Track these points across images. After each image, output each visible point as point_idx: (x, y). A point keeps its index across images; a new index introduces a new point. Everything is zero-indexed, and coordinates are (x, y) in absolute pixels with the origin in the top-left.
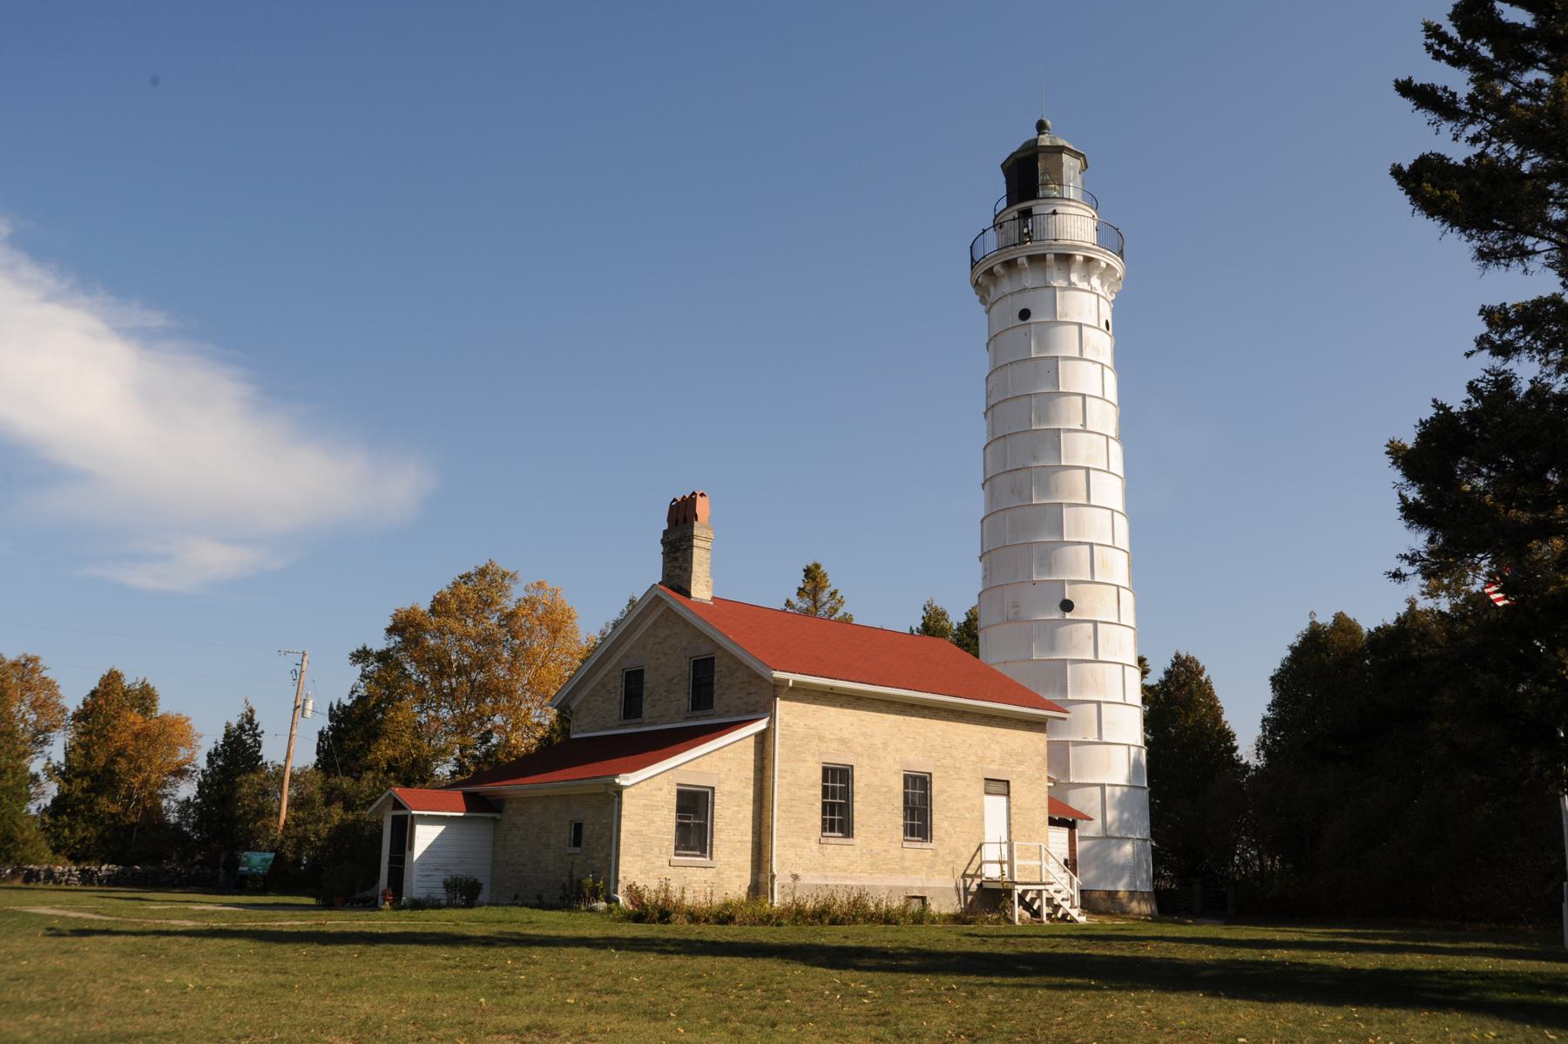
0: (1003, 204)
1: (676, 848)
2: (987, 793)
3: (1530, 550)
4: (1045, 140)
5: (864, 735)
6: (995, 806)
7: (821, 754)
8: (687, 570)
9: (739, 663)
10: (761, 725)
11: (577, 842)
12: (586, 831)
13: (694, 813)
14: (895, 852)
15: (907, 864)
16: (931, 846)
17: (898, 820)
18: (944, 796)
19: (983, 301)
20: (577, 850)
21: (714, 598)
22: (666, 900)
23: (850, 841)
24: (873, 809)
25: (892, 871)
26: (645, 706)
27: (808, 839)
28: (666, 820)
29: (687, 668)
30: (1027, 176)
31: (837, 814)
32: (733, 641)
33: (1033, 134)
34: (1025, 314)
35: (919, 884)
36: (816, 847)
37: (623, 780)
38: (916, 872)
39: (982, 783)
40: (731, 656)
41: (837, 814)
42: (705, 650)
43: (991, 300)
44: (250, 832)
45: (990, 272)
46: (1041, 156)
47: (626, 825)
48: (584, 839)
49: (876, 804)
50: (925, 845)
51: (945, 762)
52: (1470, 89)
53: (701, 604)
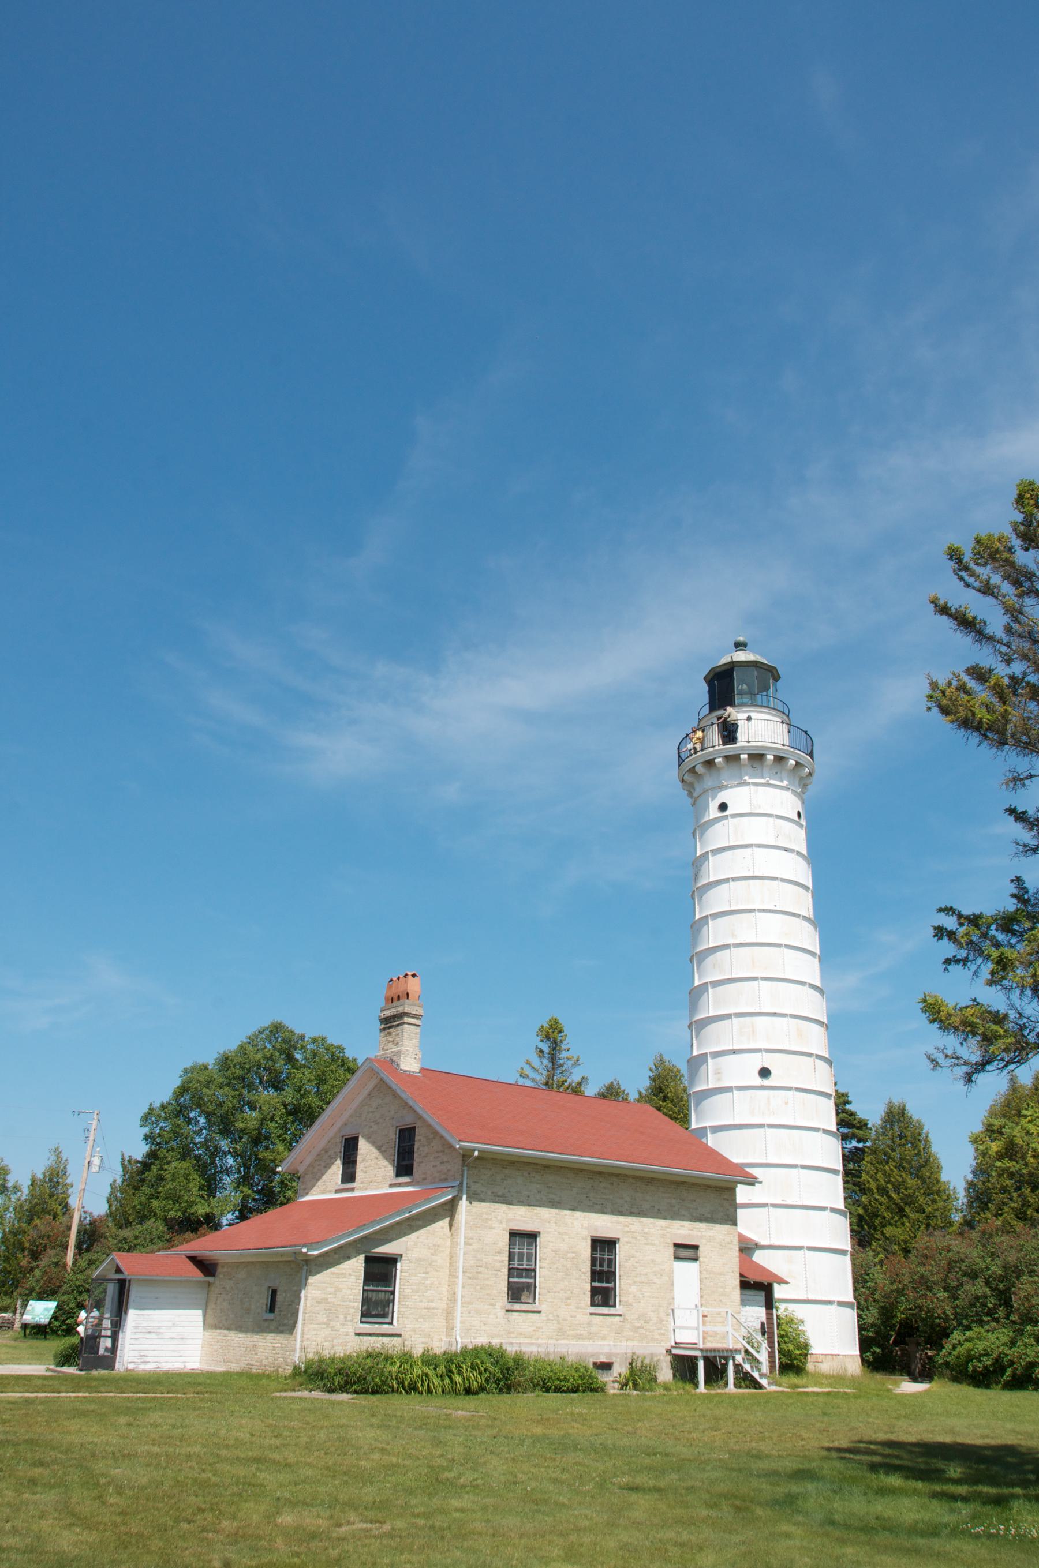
0: (706, 709)
1: (363, 1315)
2: (677, 1258)
3: (877, 1333)
6: (686, 1272)
7: (509, 1220)
9: (436, 1133)
12: (280, 1298)
15: (594, 1329)
17: (585, 1285)
18: (632, 1261)
19: (690, 794)
20: (271, 1316)
21: (422, 1070)
22: (383, 1348)
24: (560, 1275)
25: (579, 1337)
27: (493, 1305)
35: (606, 1350)
38: (604, 1338)
39: (672, 1249)
40: (429, 1126)
42: (408, 1121)
43: (695, 795)
44: (91, 1224)
45: (692, 770)
48: (278, 1305)
52: (99, 1207)
53: (408, 1075)
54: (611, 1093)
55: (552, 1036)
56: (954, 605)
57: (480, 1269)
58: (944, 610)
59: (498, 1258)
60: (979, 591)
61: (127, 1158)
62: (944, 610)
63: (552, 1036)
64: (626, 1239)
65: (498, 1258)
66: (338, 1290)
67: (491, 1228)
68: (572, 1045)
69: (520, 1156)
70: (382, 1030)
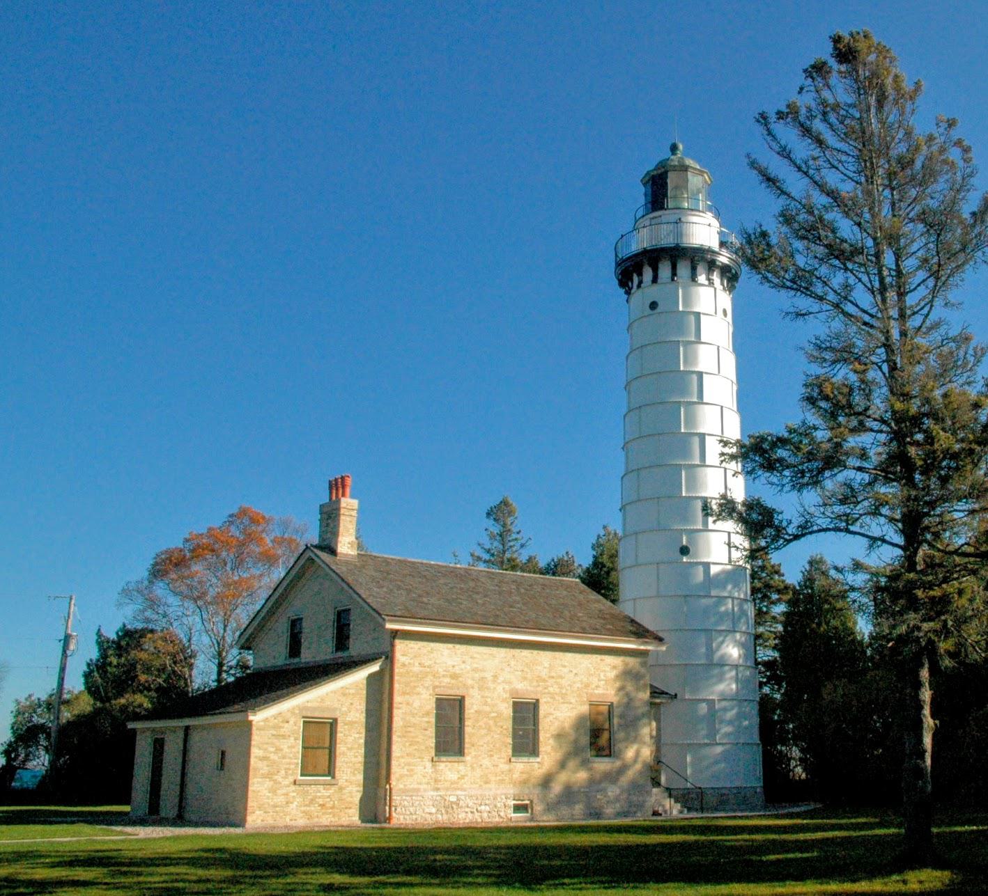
4: (675, 160)
5: (475, 670)
7: (435, 687)
8: (335, 534)
10: (375, 668)
11: (222, 765)
12: (228, 758)
13: (319, 743)
14: (504, 767)
16: (538, 760)
18: (551, 718)
23: (461, 758)
24: (483, 732)
26: (303, 650)
28: (293, 748)
29: (332, 617)
30: (337, 486)
31: (450, 733)
32: (372, 593)
33: (666, 154)
34: (653, 305)
36: (429, 764)
37: (251, 718)
41: (450, 733)
46: (670, 174)
47: (255, 752)
49: (488, 728)
50: (532, 759)
51: (551, 689)
54: (556, 568)
55: (500, 512)
56: (763, 162)
57: (409, 729)
58: (753, 164)
59: (426, 719)
60: (778, 153)
61: (810, 349)
62: (753, 164)
63: (500, 512)
64: (545, 700)
65: (426, 719)
66: (278, 750)
67: (418, 694)
68: (521, 523)
69: (421, 624)
70: (805, 71)
